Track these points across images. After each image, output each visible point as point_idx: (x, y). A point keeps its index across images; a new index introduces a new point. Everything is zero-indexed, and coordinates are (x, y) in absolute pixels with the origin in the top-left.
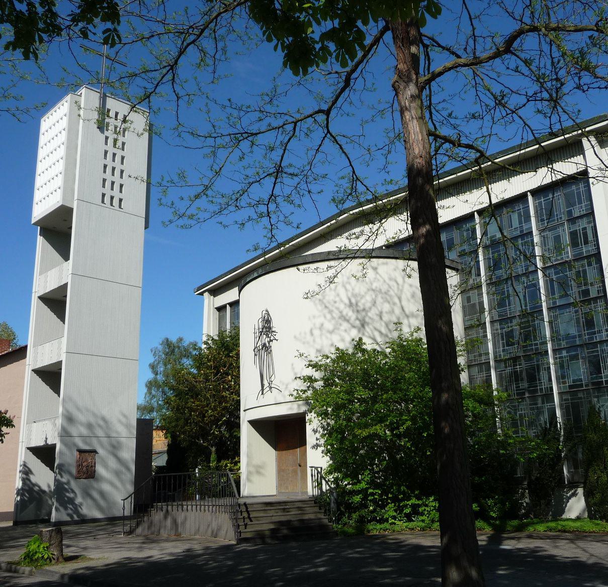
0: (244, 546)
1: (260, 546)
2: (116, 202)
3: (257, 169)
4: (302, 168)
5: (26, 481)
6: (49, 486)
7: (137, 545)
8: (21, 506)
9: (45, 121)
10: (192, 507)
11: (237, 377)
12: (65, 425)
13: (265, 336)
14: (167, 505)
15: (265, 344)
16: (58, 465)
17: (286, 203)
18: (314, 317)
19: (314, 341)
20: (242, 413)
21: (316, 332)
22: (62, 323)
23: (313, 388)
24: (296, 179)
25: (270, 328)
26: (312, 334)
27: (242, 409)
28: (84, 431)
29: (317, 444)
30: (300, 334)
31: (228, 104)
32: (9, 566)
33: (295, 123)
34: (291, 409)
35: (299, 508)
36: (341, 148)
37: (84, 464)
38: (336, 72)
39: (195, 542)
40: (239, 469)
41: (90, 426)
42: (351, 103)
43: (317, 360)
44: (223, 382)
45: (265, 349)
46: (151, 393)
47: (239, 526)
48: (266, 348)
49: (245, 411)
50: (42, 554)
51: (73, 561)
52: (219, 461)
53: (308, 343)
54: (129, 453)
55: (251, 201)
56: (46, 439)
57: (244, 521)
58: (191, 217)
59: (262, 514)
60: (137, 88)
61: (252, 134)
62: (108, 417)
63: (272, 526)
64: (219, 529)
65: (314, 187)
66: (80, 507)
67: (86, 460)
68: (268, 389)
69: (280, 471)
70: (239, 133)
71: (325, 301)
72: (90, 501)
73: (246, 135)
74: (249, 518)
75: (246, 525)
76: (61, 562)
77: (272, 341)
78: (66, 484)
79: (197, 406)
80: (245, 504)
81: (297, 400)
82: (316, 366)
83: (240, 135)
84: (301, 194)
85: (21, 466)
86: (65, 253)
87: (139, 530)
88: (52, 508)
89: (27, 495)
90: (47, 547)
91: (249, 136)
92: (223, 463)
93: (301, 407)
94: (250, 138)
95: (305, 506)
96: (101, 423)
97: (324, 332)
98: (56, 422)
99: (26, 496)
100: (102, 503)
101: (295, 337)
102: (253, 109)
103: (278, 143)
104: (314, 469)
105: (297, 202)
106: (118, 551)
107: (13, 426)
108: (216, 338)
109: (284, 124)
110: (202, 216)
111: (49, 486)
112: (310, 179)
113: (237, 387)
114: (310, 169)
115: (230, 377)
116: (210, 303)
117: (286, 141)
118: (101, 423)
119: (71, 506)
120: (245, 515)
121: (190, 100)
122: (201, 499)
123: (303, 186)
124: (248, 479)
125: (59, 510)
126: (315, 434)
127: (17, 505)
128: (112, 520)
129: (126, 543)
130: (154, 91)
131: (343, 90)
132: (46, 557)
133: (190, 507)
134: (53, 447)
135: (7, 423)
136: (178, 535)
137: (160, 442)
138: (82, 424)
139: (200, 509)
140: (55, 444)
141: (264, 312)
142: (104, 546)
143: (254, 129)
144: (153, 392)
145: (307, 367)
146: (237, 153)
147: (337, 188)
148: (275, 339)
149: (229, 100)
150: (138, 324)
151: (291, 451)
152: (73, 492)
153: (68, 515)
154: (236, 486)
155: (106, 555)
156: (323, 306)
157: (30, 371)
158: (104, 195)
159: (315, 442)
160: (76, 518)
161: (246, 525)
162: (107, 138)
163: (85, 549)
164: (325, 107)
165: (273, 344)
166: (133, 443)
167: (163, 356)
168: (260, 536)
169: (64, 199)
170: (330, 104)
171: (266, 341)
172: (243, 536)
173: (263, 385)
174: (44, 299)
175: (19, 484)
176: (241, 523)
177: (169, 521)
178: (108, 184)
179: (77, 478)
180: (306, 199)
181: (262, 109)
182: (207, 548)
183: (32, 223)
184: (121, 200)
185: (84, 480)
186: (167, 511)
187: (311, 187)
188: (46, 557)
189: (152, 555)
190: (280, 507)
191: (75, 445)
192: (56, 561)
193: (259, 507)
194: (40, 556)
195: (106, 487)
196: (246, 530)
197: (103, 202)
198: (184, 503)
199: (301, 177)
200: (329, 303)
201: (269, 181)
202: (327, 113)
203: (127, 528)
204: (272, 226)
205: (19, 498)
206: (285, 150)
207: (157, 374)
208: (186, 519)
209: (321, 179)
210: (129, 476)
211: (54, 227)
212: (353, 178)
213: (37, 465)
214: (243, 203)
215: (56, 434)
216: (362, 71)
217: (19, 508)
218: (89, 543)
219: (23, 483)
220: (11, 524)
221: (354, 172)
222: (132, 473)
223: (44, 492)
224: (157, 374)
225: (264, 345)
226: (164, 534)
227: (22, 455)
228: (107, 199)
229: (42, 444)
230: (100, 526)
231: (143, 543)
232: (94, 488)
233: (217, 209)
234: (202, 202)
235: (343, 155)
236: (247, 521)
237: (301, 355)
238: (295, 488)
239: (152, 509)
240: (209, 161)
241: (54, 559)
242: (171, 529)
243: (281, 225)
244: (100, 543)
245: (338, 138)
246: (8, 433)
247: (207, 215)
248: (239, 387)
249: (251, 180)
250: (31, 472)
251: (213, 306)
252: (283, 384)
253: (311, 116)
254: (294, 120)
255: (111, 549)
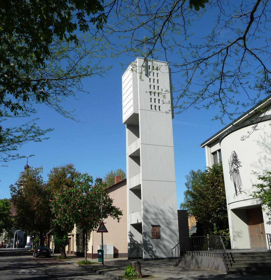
0: (231, 276)
1: (239, 276)
2: (157, 108)
3: (211, 77)
4: (235, 72)
5: (131, 239)
6: (141, 242)
7: (177, 272)
8: (130, 251)
9: (123, 77)
10: (204, 254)
11: (223, 187)
12: (145, 214)
13: (235, 165)
14: (192, 253)
15: (235, 169)
16: (143, 232)
17: (229, 92)
18: (260, 153)
19: (262, 166)
20: (228, 205)
21: (263, 161)
22: (139, 166)
23: (264, 190)
24: (233, 78)
25: (237, 160)
26: (260, 162)
27: (227, 204)
28: (153, 216)
29: (269, 221)
30: (253, 163)
31: (190, 46)
32: (119, 278)
33: (227, 48)
34: (253, 203)
35: (261, 257)
36: (255, 56)
37: (155, 232)
38: (245, 15)
39: (206, 272)
40: (229, 235)
41: (156, 214)
42: (259, 31)
43: (264, 175)
44: (217, 190)
45: (235, 171)
46: (187, 198)
47: (228, 265)
48: (236, 171)
49: (229, 204)
50: (132, 273)
51: (146, 278)
52: (218, 230)
53: (258, 167)
54: (175, 226)
55: (210, 94)
56: (138, 220)
57: (230, 262)
58: (180, 107)
59: (240, 259)
60: (146, 48)
61: (205, 59)
62: (164, 209)
63: (246, 266)
64: (219, 266)
65: (243, 81)
66: (155, 252)
67: (156, 230)
68: (239, 192)
69: (251, 236)
70: (198, 60)
71: (265, 143)
72: (159, 250)
73: (201, 61)
74: (233, 260)
75: (231, 265)
76: (141, 278)
77: (238, 167)
78: (148, 241)
79: (204, 202)
80: (231, 253)
81: (255, 197)
82: (263, 178)
83: (199, 61)
84: (237, 86)
85: (129, 232)
86: (137, 134)
87: (180, 264)
88: (143, 252)
89: (133, 246)
90: (134, 270)
91: (203, 61)
92: (221, 231)
93: (258, 202)
94: (204, 62)
95: (264, 255)
96: (161, 212)
97: (267, 160)
98: (141, 212)
99: (132, 247)
100: (165, 250)
101: (251, 165)
102: (203, 46)
103: (220, 61)
104: (269, 235)
105: (235, 90)
106: (168, 274)
107: (122, 215)
108: (211, 168)
109: (221, 50)
110: (186, 105)
111: (141, 242)
112: (241, 76)
113: (224, 192)
114: (239, 71)
115: (219, 187)
116: (208, 151)
117: (223, 59)
118: (161, 212)
119: (151, 252)
120: (231, 259)
121: (172, 49)
122: (210, 250)
123: (237, 81)
124: (234, 239)
125: (146, 253)
126: (268, 216)
127: (129, 250)
128: (171, 259)
129: (172, 271)
130: (153, 49)
131: (250, 23)
132: (134, 275)
133: (203, 254)
134: (141, 224)
135: (120, 213)
136: (199, 268)
137: (192, 222)
138: (152, 213)
139: (212, 255)
140: (142, 223)
141: (233, 152)
142: (162, 271)
143: (206, 56)
144: (188, 197)
145: (259, 179)
146: (198, 71)
147: (257, 79)
148: (240, 166)
149: (190, 44)
150: (174, 164)
151: (256, 225)
152: (151, 245)
153: (150, 256)
154: (76, 240)
155: (161, 276)
156: (265, 146)
157: (129, 190)
158: (151, 106)
159: (268, 220)
160: (153, 257)
161: (231, 265)
162: (150, 79)
163: (153, 272)
164: (242, 36)
165: (240, 169)
166: (177, 222)
167: (192, 179)
168: (239, 271)
169: (134, 110)
170: (244, 33)
171: (236, 167)
172: (230, 270)
173: (236, 191)
174: (132, 157)
175: (129, 241)
176: (229, 263)
177: (194, 261)
178: (153, 100)
179: (152, 238)
180: (240, 89)
181: (208, 45)
182: (211, 276)
183: (123, 122)
184: (159, 107)
185: (155, 239)
186: (193, 255)
187: (241, 81)
188: (134, 275)
189: (183, 277)
190: (250, 256)
191: (150, 223)
192: (138, 277)
193: (238, 255)
194: (131, 274)
195: (166, 243)
196: (231, 267)
197: (151, 109)
198: (200, 252)
199: (235, 76)
200: (268, 144)
201: (218, 82)
202: (244, 38)
203: (175, 263)
204: (223, 105)
205: (129, 247)
206: (224, 64)
207: (189, 188)
208: (202, 260)
209: (247, 76)
210: (177, 237)
211: (133, 124)
212: (265, 72)
213: (135, 232)
214: (206, 96)
215: (142, 219)
216: (263, 11)
217: (130, 251)
218: (156, 269)
219: (130, 240)
220: (127, 259)
221: (265, 68)
222: (177, 237)
223: (139, 244)
224: (189, 188)
225: (235, 170)
226: (192, 267)
227: (129, 228)
228: (153, 107)
229: (136, 223)
230: (164, 261)
231: (181, 271)
232: (161, 244)
233: (191, 101)
234: (185, 99)
235: (257, 59)
236: (232, 262)
237: (255, 173)
238: (261, 245)
239: (185, 254)
240: (185, 78)
241: (138, 276)
242: (195, 265)
243: (228, 104)
244: (161, 270)
245: (253, 51)
246: (121, 218)
247: (189, 105)
248: (225, 192)
249: (208, 83)
250: (133, 236)
251: (210, 152)
252: (247, 190)
253: (235, 42)
254: (226, 47)
255: (165, 273)
